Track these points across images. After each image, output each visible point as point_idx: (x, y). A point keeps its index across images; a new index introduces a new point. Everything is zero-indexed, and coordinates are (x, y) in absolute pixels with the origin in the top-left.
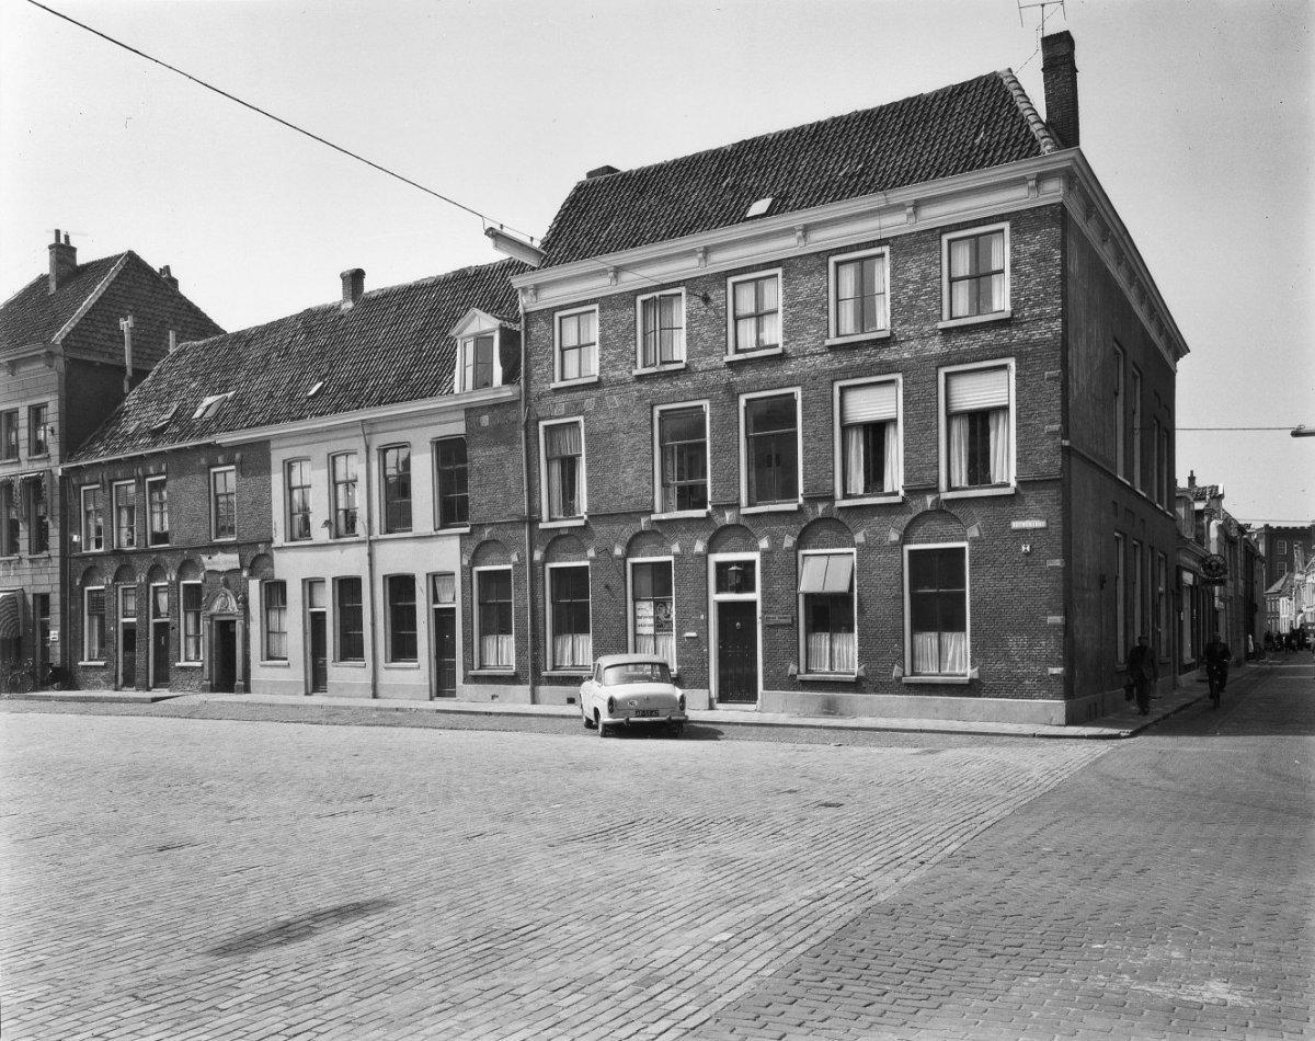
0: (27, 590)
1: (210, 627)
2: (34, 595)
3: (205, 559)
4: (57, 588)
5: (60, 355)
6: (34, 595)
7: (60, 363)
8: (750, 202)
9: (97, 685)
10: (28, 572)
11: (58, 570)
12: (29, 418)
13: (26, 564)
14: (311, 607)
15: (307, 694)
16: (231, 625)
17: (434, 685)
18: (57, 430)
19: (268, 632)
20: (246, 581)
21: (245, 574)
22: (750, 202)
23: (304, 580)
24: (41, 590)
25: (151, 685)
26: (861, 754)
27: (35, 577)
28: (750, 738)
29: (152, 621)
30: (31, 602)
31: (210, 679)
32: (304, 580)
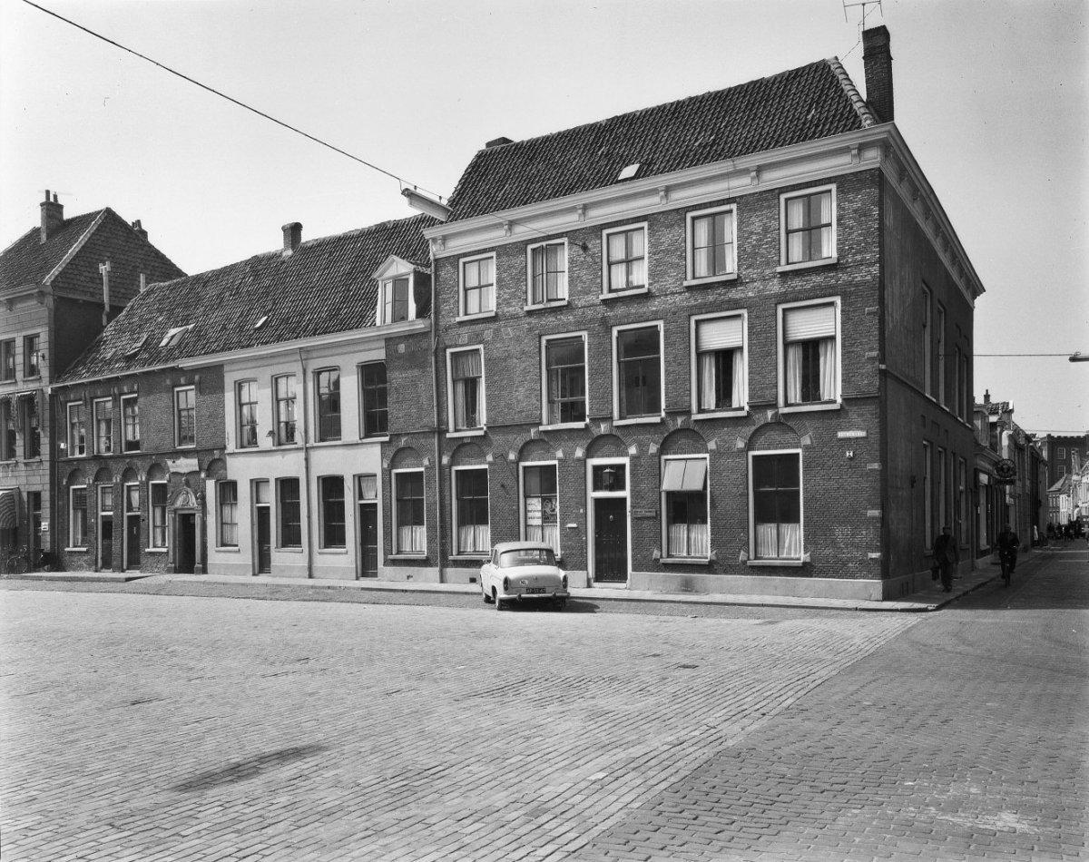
0: (22, 489)
1: (174, 519)
2: (29, 493)
3: (170, 463)
4: (47, 487)
5: (49, 294)
6: (29, 493)
7: (49, 301)
8: (621, 167)
9: (80, 568)
10: (23, 474)
11: (48, 472)
12: (24, 346)
13: (22, 467)
14: (257, 503)
15: (254, 575)
16: (191, 518)
17: (359, 567)
18: (47, 356)
19: (222, 524)
20: (204, 481)
21: (203, 475)
22: (621, 167)
23: (251, 481)
24: (34, 489)
25: (125, 567)
27: (29, 478)
29: (126, 514)
30: (25, 498)
31: (174, 562)
32: (251, 481)
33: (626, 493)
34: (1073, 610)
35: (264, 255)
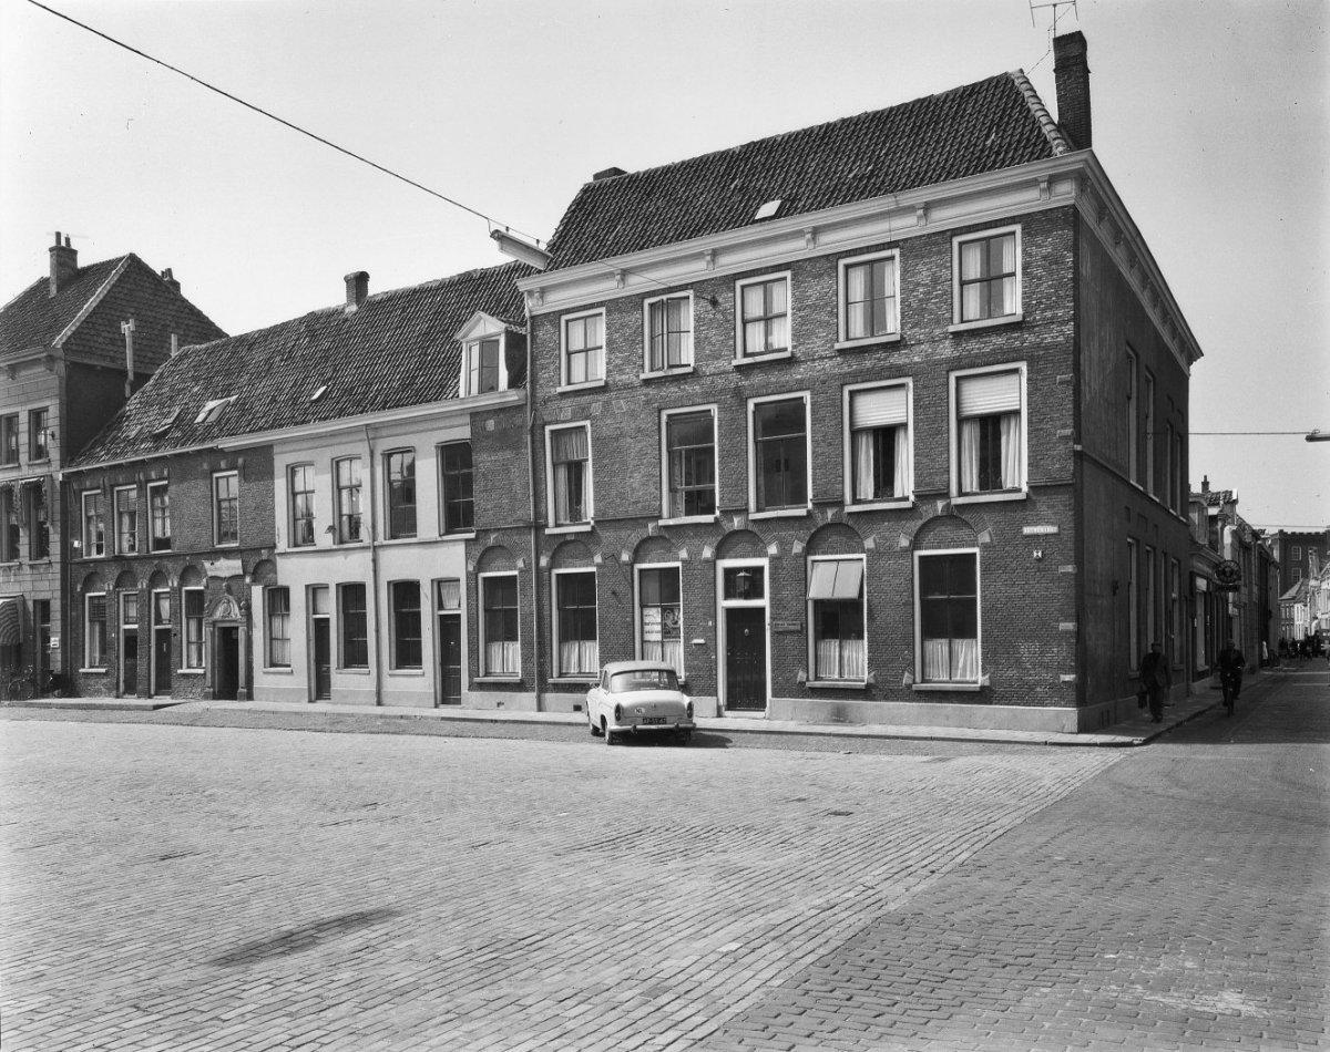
0: (27, 597)
1: (213, 634)
2: (35, 601)
3: (207, 565)
4: (58, 594)
5: (60, 358)
6: (35, 601)
7: (60, 367)
9: (98, 693)
10: (28, 578)
11: (59, 576)
12: (29, 422)
13: (27, 570)
14: (314, 613)
15: (310, 701)
16: (234, 632)
17: (439, 692)
18: (57, 435)
19: (271, 639)
20: (249, 587)
21: (248, 580)
23: (307, 587)
24: (41, 596)
25: (152, 692)
26: (870, 762)
27: (35, 584)
28: (758, 745)
29: (154, 628)
30: (31, 608)
31: (213, 686)
32: (307, 587)
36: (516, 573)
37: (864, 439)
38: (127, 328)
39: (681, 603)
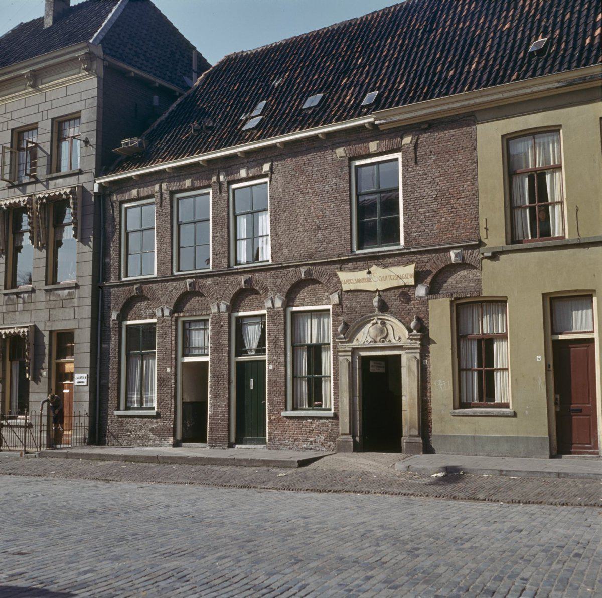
0: (41, 327)
1: (351, 365)
2: (51, 332)
3: (343, 276)
4: (87, 323)
5: (99, 57)
6: (51, 332)
7: (98, 66)
8: (203, 86)
9: (143, 440)
10: (42, 305)
11: (88, 301)
12: (52, 132)
13: (40, 296)
14: (238, 354)
15: (552, 456)
16: (373, 368)
17: (554, 438)
18: (93, 141)
19: (460, 370)
20: (424, 302)
21: (421, 291)
22: (203, 86)
23: (544, 295)
24: (60, 326)
25: (233, 440)
26: (129, 491)
27: (53, 312)
28: (159, 480)
29: (234, 359)
30: (46, 340)
31: (352, 433)
32: (544, 295)
33: (266, 357)
34: (210, 456)
35: (287, 40)
36: (154, 320)
37: (242, 219)
38: (91, 41)
39: (267, 347)
